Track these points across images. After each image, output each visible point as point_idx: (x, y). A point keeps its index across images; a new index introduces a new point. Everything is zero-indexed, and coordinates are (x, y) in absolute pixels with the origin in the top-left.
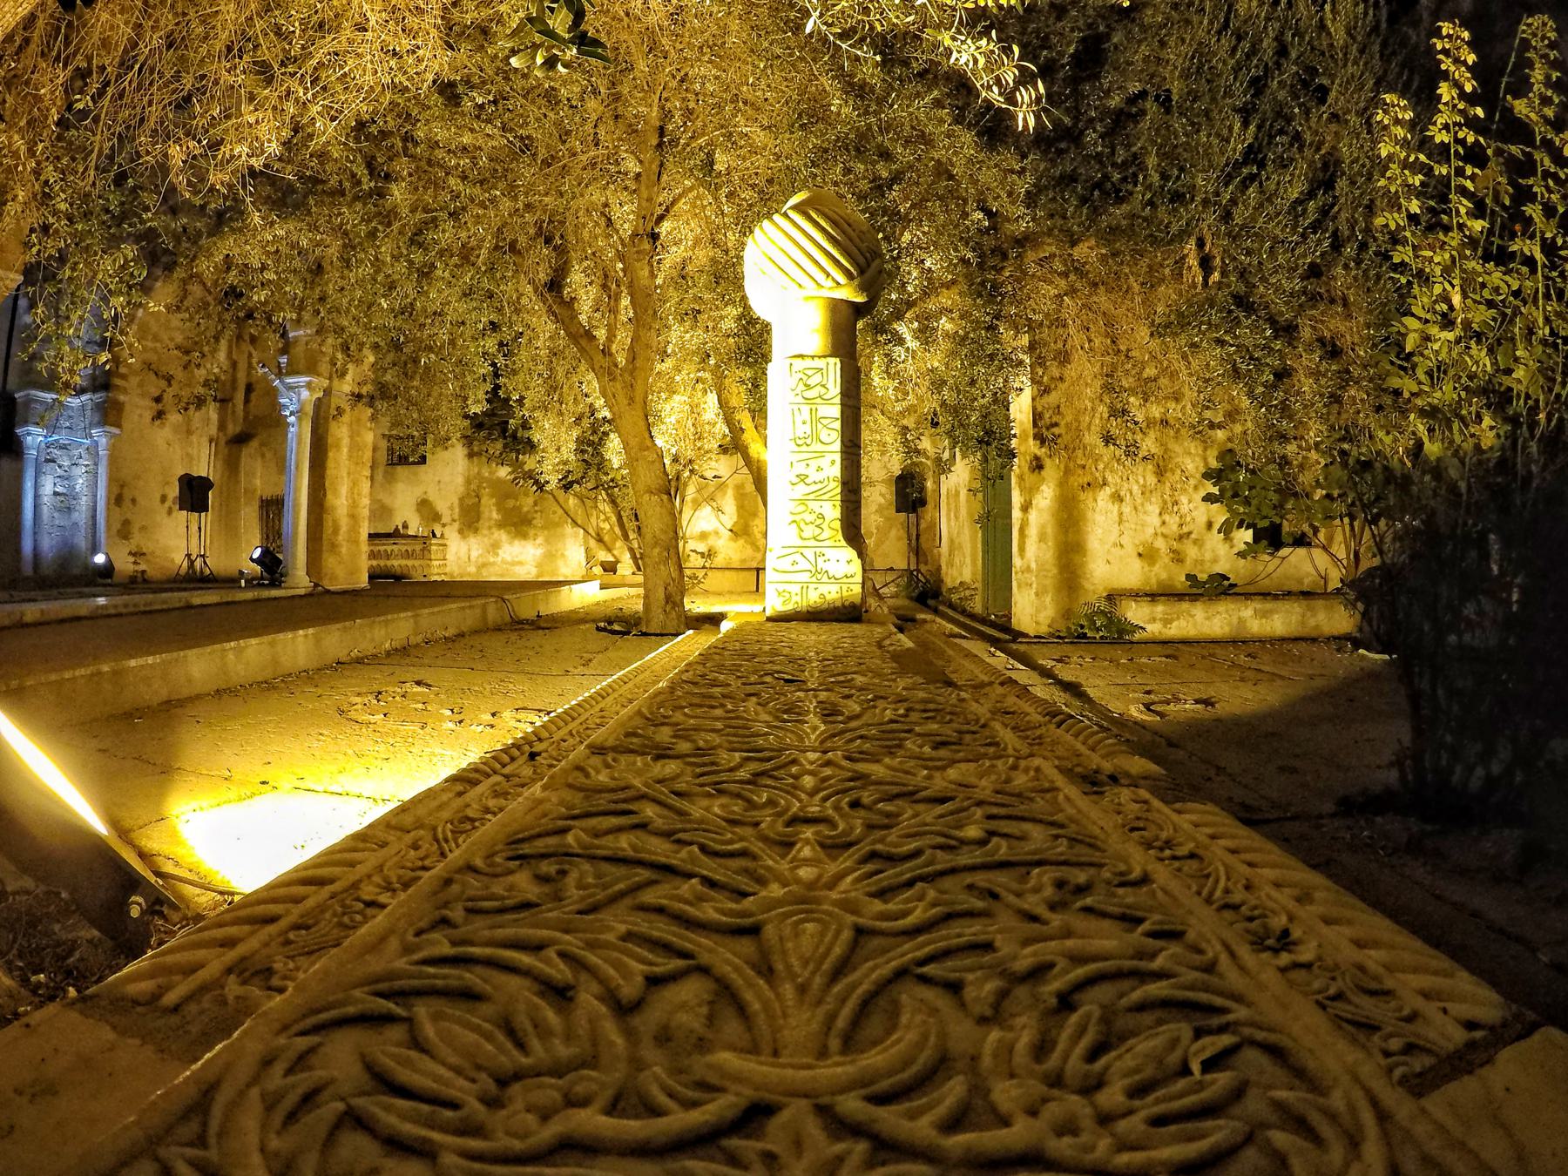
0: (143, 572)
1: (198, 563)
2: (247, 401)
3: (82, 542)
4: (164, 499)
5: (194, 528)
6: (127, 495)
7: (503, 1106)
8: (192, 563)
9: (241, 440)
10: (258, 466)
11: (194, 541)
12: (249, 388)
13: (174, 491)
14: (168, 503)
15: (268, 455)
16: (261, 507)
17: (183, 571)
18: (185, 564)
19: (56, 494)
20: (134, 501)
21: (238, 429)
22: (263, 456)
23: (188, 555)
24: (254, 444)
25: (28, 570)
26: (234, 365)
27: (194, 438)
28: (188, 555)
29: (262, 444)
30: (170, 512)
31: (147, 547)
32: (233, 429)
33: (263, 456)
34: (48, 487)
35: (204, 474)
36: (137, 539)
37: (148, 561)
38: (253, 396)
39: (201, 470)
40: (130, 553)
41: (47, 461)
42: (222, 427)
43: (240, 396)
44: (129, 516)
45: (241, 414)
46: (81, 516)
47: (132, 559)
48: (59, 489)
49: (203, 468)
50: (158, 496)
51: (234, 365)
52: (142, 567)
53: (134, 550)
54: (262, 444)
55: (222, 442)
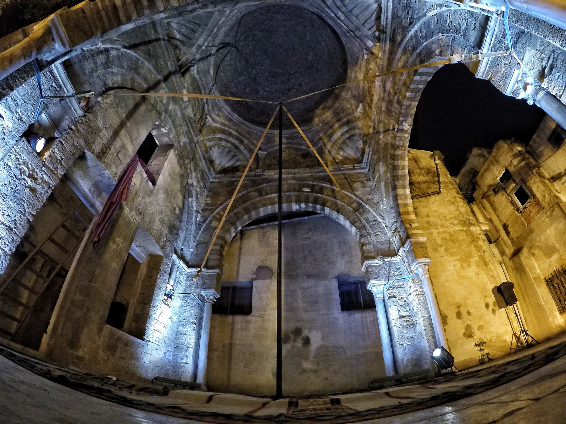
0: (488, 354)
1: (523, 338)
2: (508, 233)
3: (425, 344)
4: (487, 306)
5: (513, 316)
6: (464, 311)
7: (478, 173)
8: (518, 338)
9: (517, 252)
10: (533, 261)
11: (515, 324)
12: (505, 227)
13: (492, 299)
14: (491, 308)
15: (536, 251)
16: (548, 285)
17: (514, 346)
18: (514, 340)
19: (401, 317)
20: (469, 313)
21: (512, 251)
22: (533, 254)
23: (515, 334)
24: (525, 251)
25: (390, 372)
26: (491, 221)
27: (490, 265)
28: (515, 334)
29: (530, 248)
30: (494, 312)
31: (486, 337)
32: (509, 251)
33: (533, 254)
34: (394, 314)
35: (504, 280)
36: (478, 336)
37: (489, 346)
38: (510, 229)
39: (503, 279)
40: (476, 345)
41: (389, 298)
42: (502, 253)
43: (503, 233)
44: (469, 323)
45: (509, 242)
46: (421, 326)
47: (478, 348)
48: (404, 314)
49: (502, 276)
50: (483, 306)
51: (491, 221)
52: (486, 351)
53: (478, 342)
54: (530, 248)
55: (507, 260)
